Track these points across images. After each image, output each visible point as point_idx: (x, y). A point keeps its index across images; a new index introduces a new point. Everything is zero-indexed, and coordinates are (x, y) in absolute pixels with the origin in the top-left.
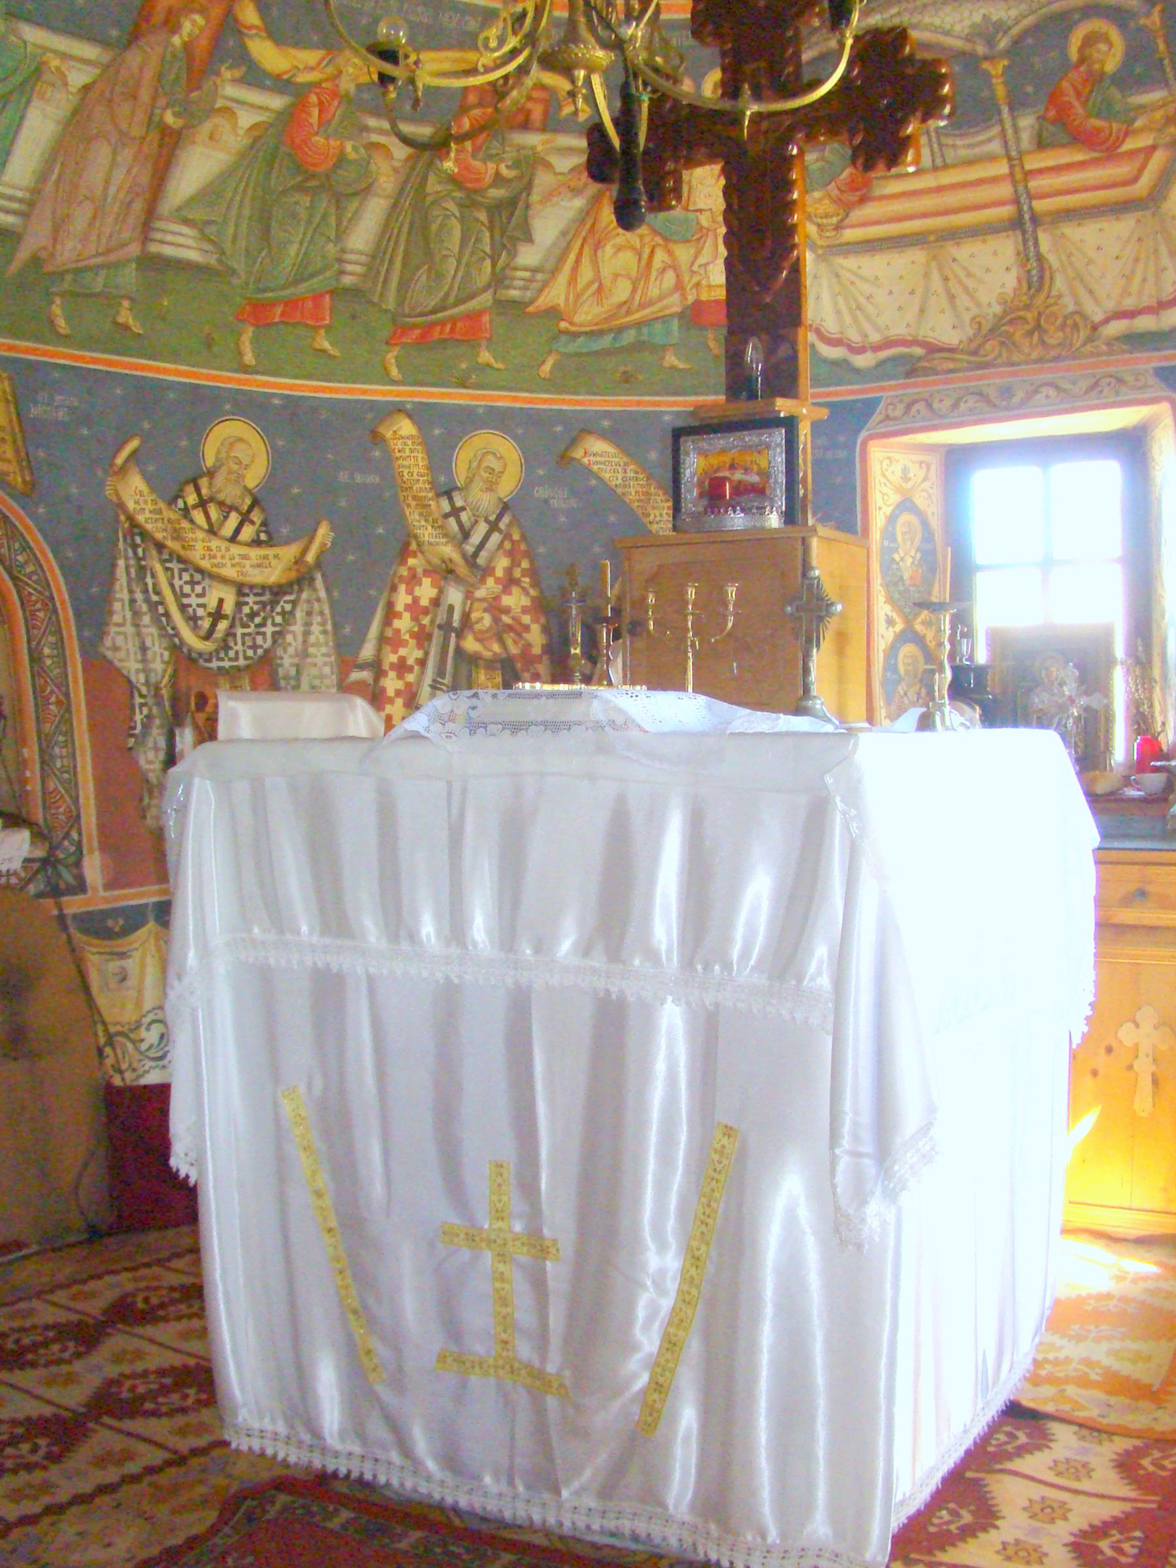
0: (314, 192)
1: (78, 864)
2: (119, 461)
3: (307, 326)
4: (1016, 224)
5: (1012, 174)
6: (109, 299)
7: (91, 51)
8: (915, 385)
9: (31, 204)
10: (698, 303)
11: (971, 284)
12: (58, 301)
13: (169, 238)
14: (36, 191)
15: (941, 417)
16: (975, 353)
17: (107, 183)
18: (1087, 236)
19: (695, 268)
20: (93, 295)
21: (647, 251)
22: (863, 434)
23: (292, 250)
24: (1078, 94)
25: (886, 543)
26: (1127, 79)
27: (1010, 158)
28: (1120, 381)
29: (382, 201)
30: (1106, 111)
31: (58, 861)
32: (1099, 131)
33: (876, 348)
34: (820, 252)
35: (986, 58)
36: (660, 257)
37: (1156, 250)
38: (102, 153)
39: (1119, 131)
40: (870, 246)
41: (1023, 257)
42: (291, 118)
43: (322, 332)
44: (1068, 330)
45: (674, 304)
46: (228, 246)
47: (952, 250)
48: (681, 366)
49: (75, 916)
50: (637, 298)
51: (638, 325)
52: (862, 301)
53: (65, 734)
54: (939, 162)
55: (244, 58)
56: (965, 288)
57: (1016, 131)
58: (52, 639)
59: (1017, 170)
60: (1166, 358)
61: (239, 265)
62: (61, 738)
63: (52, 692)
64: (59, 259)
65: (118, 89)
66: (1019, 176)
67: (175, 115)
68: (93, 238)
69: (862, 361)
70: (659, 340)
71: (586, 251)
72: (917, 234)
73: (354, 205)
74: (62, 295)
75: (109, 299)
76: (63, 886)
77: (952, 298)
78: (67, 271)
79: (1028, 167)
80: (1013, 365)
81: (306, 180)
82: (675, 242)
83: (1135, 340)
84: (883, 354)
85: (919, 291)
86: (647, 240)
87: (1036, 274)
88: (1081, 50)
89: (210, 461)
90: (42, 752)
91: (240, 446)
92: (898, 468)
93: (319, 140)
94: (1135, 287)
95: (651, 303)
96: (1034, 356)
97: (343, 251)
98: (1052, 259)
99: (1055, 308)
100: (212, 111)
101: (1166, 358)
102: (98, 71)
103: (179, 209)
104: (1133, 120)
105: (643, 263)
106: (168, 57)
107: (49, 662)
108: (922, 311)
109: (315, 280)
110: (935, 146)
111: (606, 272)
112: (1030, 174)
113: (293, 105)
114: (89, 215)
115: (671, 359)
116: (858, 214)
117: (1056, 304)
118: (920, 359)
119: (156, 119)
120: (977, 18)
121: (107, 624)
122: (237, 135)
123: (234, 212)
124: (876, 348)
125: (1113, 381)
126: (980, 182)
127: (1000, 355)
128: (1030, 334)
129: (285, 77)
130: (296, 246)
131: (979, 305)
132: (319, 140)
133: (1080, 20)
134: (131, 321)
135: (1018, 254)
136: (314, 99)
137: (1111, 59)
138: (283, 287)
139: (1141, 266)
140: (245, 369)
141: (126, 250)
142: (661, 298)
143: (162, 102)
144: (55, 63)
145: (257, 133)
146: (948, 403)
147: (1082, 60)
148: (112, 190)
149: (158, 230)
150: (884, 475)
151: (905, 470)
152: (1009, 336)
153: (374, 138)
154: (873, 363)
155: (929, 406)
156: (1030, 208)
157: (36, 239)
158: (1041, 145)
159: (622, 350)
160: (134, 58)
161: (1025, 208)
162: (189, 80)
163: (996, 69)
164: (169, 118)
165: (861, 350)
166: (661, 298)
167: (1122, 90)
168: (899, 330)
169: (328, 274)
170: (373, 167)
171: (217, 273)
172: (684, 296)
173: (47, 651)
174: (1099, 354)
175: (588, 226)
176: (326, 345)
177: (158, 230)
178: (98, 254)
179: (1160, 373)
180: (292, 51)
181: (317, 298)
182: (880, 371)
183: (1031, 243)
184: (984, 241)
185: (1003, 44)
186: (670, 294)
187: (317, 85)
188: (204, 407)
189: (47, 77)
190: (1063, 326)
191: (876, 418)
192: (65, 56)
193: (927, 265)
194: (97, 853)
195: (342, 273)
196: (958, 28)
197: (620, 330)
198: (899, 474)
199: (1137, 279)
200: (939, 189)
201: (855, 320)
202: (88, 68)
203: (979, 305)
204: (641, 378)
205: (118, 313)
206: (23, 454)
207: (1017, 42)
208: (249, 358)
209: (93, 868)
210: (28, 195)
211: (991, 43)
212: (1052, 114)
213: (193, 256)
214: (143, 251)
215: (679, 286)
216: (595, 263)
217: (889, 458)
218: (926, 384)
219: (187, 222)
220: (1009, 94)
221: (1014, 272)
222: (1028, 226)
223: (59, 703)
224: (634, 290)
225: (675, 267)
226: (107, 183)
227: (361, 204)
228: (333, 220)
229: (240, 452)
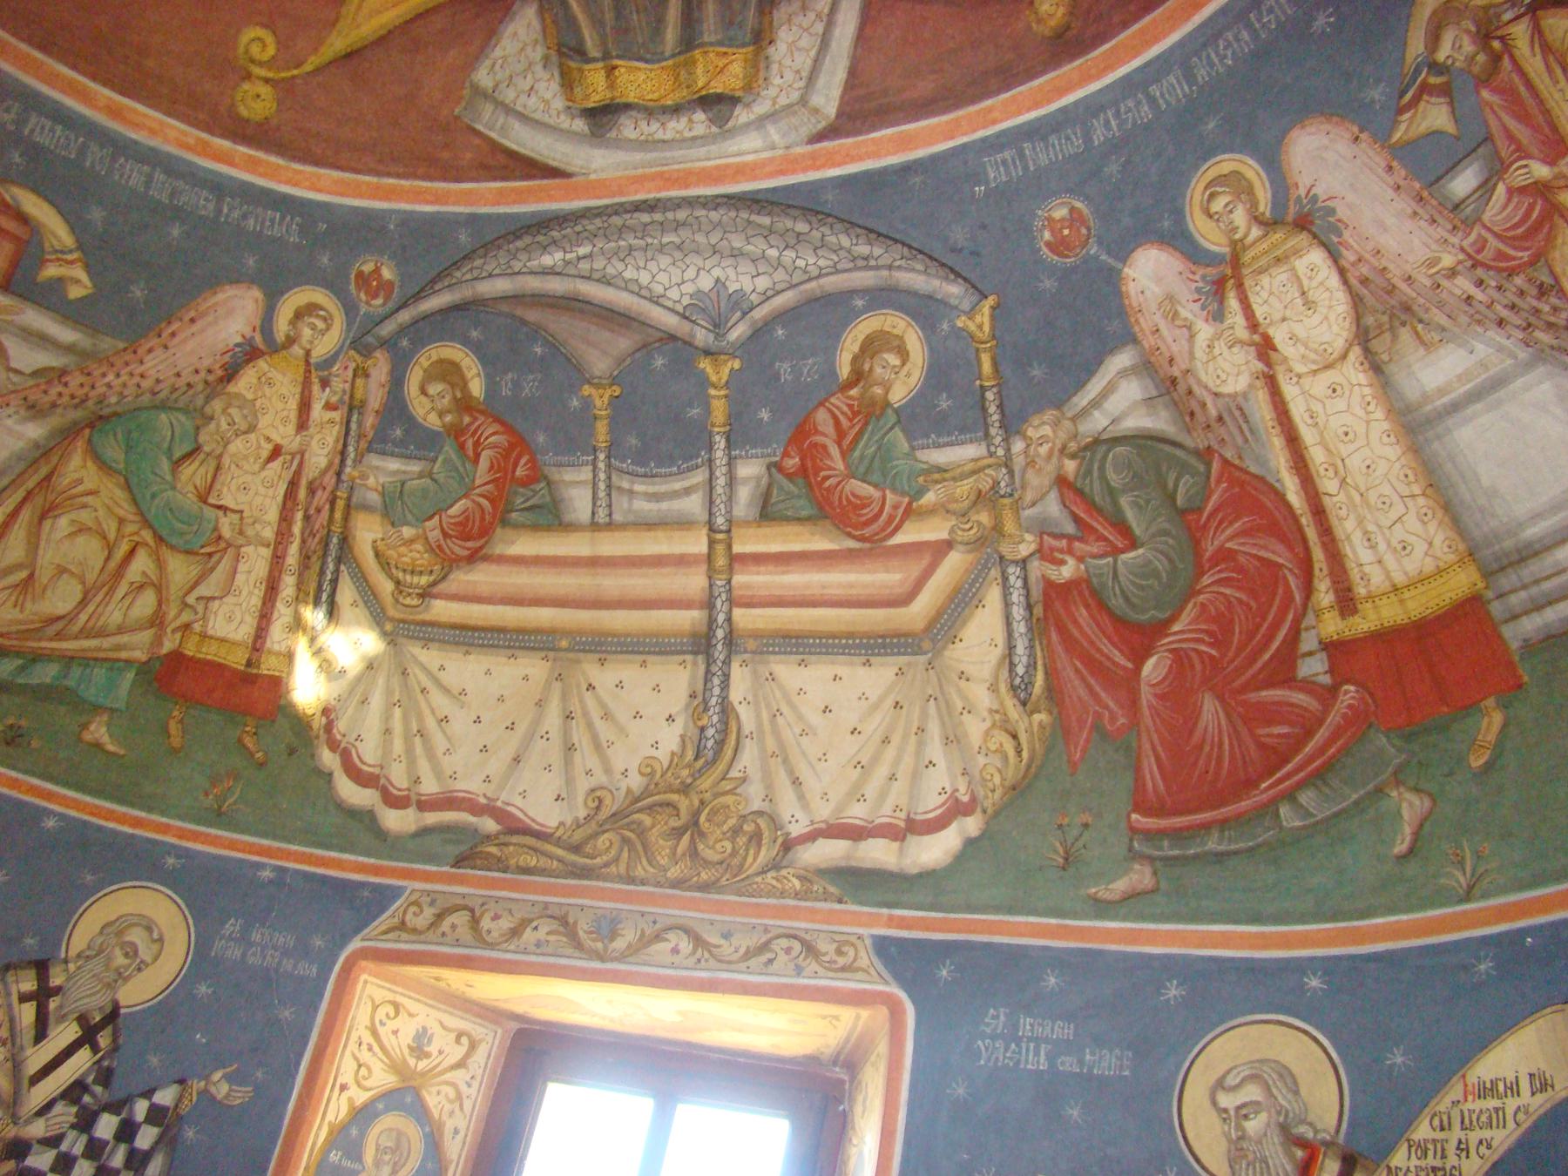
4: (700, 643)
5: (710, 558)
8: (462, 881)
10: (177, 657)
11: (604, 730)
15: (491, 946)
16: (576, 849)
18: (811, 683)
19: (191, 600)
21: (124, 548)
22: (356, 944)
24: (841, 434)
25: (334, 1157)
26: (923, 419)
27: (712, 530)
28: (810, 949)
30: (879, 469)
32: (865, 503)
33: (424, 805)
34: (388, 627)
35: (707, 353)
36: (142, 564)
37: (921, 730)
39: (896, 507)
40: (468, 637)
41: (698, 702)
44: (741, 841)
45: (138, 646)
47: (591, 669)
48: (111, 748)
50: (83, 617)
51: (69, 660)
52: (431, 723)
54: (602, 516)
56: (595, 738)
57: (732, 482)
59: (720, 548)
60: (903, 923)
66: (721, 561)
69: (396, 821)
70: (90, 693)
71: (26, 515)
72: (538, 631)
77: (570, 748)
79: (737, 548)
80: (631, 880)
82: (172, 547)
83: (857, 882)
84: (432, 818)
85: (521, 728)
86: (130, 528)
87: (714, 735)
88: (856, 359)
92: (407, 1029)
94: (871, 790)
95: (102, 633)
96: (674, 872)
98: (745, 713)
99: (729, 799)
101: (903, 923)
104: (921, 492)
105: (113, 564)
108: (517, 760)
110: (602, 486)
111: (48, 557)
112: (735, 560)
115: (99, 731)
116: (462, 578)
117: (731, 792)
118: (488, 838)
120: (706, 283)
124: (424, 805)
125: (797, 946)
126: (658, 561)
127: (616, 860)
128: (678, 833)
131: (608, 770)
133: (867, 309)
135: (693, 696)
137: (902, 382)
139: (890, 752)
142: (121, 630)
146: (505, 924)
147: (858, 376)
150: (375, 1033)
151: (422, 1037)
152: (642, 832)
154: (413, 828)
155: (475, 921)
156: (729, 620)
158: (767, 513)
159: (25, 689)
161: (721, 618)
163: (718, 373)
165: (396, 802)
166: (121, 630)
167: (910, 437)
168: (471, 785)
172: (158, 641)
174: (783, 894)
175: (44, 471)
179: (882, 946)
182: (422, 843)
183: (716, 681)
184: (644, 664)
185: (738, 332)
186: (141, 628)
190: (736, 831)
191: (385, 920)
193: (547, 686)
196: (674, 294)
197: (37, 658)
198: (406, 1038)
199: (882, 771)
200: (594, 562)
201: (409, 750)
203: (608, 770)
204: (35, 744)
207: (760, 332)
211: (718, 326)
212: (792, 462)
215: (157, 621)
216: (33, 545)
217: (397, 1007)
218: (480, 882)
220: (733, 418)
221: (678, 727)
222: (719, 652)
224: (84, 603)
225: (159, 588)
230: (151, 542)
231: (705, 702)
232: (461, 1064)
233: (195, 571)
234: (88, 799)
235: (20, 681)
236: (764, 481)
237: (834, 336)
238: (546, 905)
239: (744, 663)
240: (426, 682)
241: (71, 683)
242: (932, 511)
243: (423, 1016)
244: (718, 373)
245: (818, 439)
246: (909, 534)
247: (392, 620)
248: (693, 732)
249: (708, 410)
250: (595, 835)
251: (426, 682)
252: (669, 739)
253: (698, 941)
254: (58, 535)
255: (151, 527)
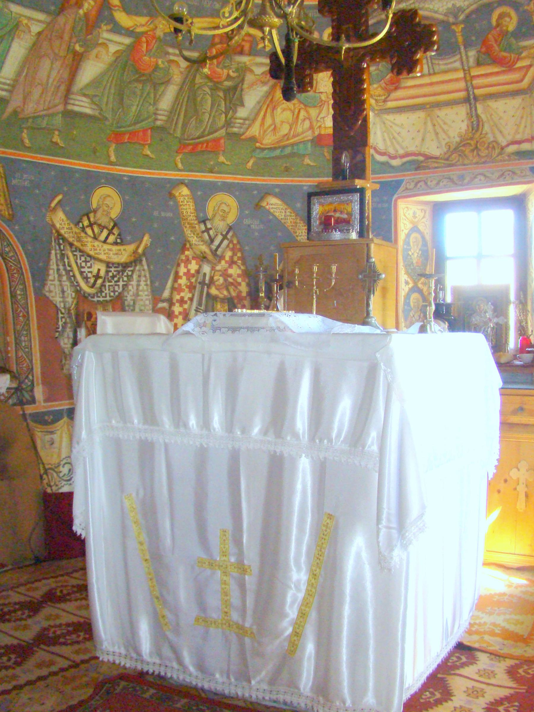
0: (144, 82)
1: (32, 390)
2: (53, 205)
3: (140, 144)
4: (466, 100)
5: (465, 77)
6: (49, 131)
7: (41, 16)
8: (419, 174)
9: (14, 86)
10: (320, 135)
11: (445, 127)
12: (25, 131)
13: (77, 103)
14: (16, 80)
15: (431, 189)
16: (447, 159)
17: (49, 77)
19: (319, 119)
20: (41, 129)
21: (297, 111)
22: (395, 196)
23: (134, 109)
24: (496, 41)
25: (405, 247)
26: (518, 34)
27: (464, 70)
29: (175, 87)
30: (508, 48)
31: (23, 389)
32: (505, 58)
33: (402, 157)
34: (376, 112)
35: (454, 24)
36: (303, 114)
38: (46, 64)
39: (514, 58)
40: (400, 110)
41: (470, 116)
42: (134, 48)
43: (147, 147)
44: (490, 149)
45: (309, 135)
46: (104, 106)
47: (437, 112)
49: (30, 414)
50: (292, 133)
51: (293, 145)
52: (396, 135)
53: (27, 331)
54: (431, 71)
55: (112, 20)
57: (467, 57)
58: (21, 287)
59: (468, 75)
61: (109, 115)
62: (25, 333)
63: (21, 311)
64: (26, 112)
65: (54, 34)
66: (468, 78)
67: (80, 46)
68: (42, 102)
69: (395, 163)
70: (302, 152)
71: (269, 111)
73: (162, 88)
74: (27, 128)
75: (49, 131)
76: (25, 400)
77: (437, 134)
78: (30, 118)
79: (472, 74)
80: (464, 165)
81: (140, 77)
82: (310, 107)
84: (405, 160)
85: (422, 131)
86: (297, 106)
87: (476, 124)
88: (497, 21)
89: (94, 206)
90: (16, 339)
91: (109, 199)
92: (411, 212)
93: (146, 58)
94: (521, 130)
95: (298, 135)
96: (474, 161)
97: (157, 109)
98: (483, 117)
99: (484, 139)
100: (97, 45)
102: (45, 26)
103: (82, 89)
104: (521, 53)
105: (295, 116)
106: (77, 19)
107: (19, 297)
109: (144, 123)
110: (430, 64)
111: (278, 120)
113: (134, 42)
114: (40, 92)
115: (307, 161)
116: (394, 95)
117: (484, 137)
118: (422, 162)
119: (71, 48)
120: (450, 5)
121: (46, 280)
122: (108, 56)
123: (107, 91)
124: (402, 157)
127: (459, 160)
128: (473, 151)
129: (131, 29)
130: (135, 107)
132: (146, 58)
133: (497, 7)
134: (59, 141)
135: (468, 114)
136: (144, 39)
138: (129, 126)
140: (111, 163)
141: (57, 108)
142: (303, 133)
143: (74, 40)
144: (25, 22)
145: (118, 55)
146: (434, 182)
147: (498, 25)
148: (51, 80)
149: (72, 99)
150: (405, 215)
151: (414, 213)
152: (463, 152)
153: (172, 58)
155: (426, 184)
156: (473, 93)
157: (16, 102)
158: (479, 64)
160: (61, 20)
161: (471, 93)
162: (87, 30)
163: (458, 29)
164: (77, 48)
166: (303, 133)
167: (516, 39)
168: (412, 149)
169: (150, 120)
170: (171, 71)
171: (99, 119)
172: (313, 132)
173: (18, 292)
176: (149, 153)
177: (72, 99)
178: (44, 110)
180: (134, 17)
181: (145, 131)
182: (403, 167)
183: (473, 109)
184: (452, 108)
185: (462, 17)
187: (146, 33)
188: (92, 181)
189: (21, 28)
190: (488, 147)
191: (401, 189)
192: (30, 19)
193: (426, 119)
194: (41, 386)
195: (156, 119)
196: (441, 10)
197: (284, 147)
198: (411, 215)
199: (522, 126)
202: (40, 24)
203: (449, 137)
204: (293, 169)
205: (53, 137)
206: (8, 202)
207: (468, 16)
208: (113, 158)
209: (39, 392)
210: (12, 82)
211: (456, 17)
212: (484, 50)
213: (88, 111)
214: (65, 109)
215: (311, 127)
216: (273, 116)
217: (407, 208)
219: (85, 95)
221: (466, 123)
222: (472, 101)
223: (24, 316)
224: (291, 129)
225: (310, 119)
226: (49, 77)
227: (165, 88)
228: (152, 95)
229: (108, 201)
230: (303, 107)
231: (471, 115)
232: (424, 217)
233: (318, 111)
234: (311, 179)
235: (283, 154)
236: (477, 56)
237: (490, 13)
238: (444, 176)
239: (480, 103)
240: (391, 124)
241: (295, 151)
242: (525, 58)
243: (414, 208)
244: (458, 29)
245: (490, 43)
246: (519, 65)
247: (377, 110)
248: (470, 124)
249: (456, 39)
250: (452, 155)
251: (391, 124)
252: (464, 126)
253: (485, 176)
254: (278, 113)
255: (303, 103)
